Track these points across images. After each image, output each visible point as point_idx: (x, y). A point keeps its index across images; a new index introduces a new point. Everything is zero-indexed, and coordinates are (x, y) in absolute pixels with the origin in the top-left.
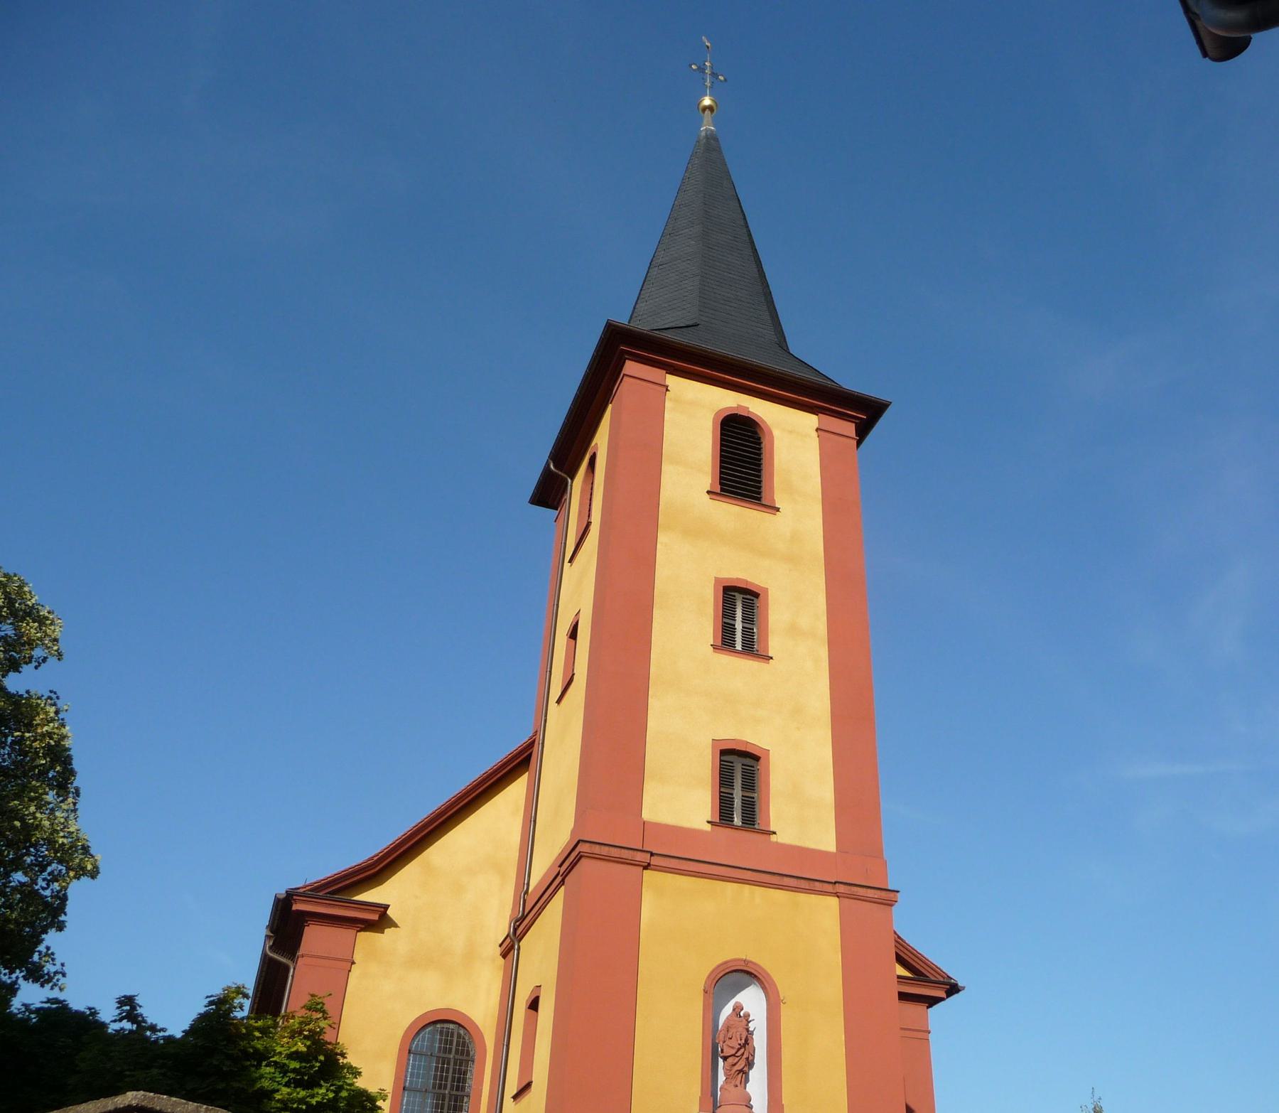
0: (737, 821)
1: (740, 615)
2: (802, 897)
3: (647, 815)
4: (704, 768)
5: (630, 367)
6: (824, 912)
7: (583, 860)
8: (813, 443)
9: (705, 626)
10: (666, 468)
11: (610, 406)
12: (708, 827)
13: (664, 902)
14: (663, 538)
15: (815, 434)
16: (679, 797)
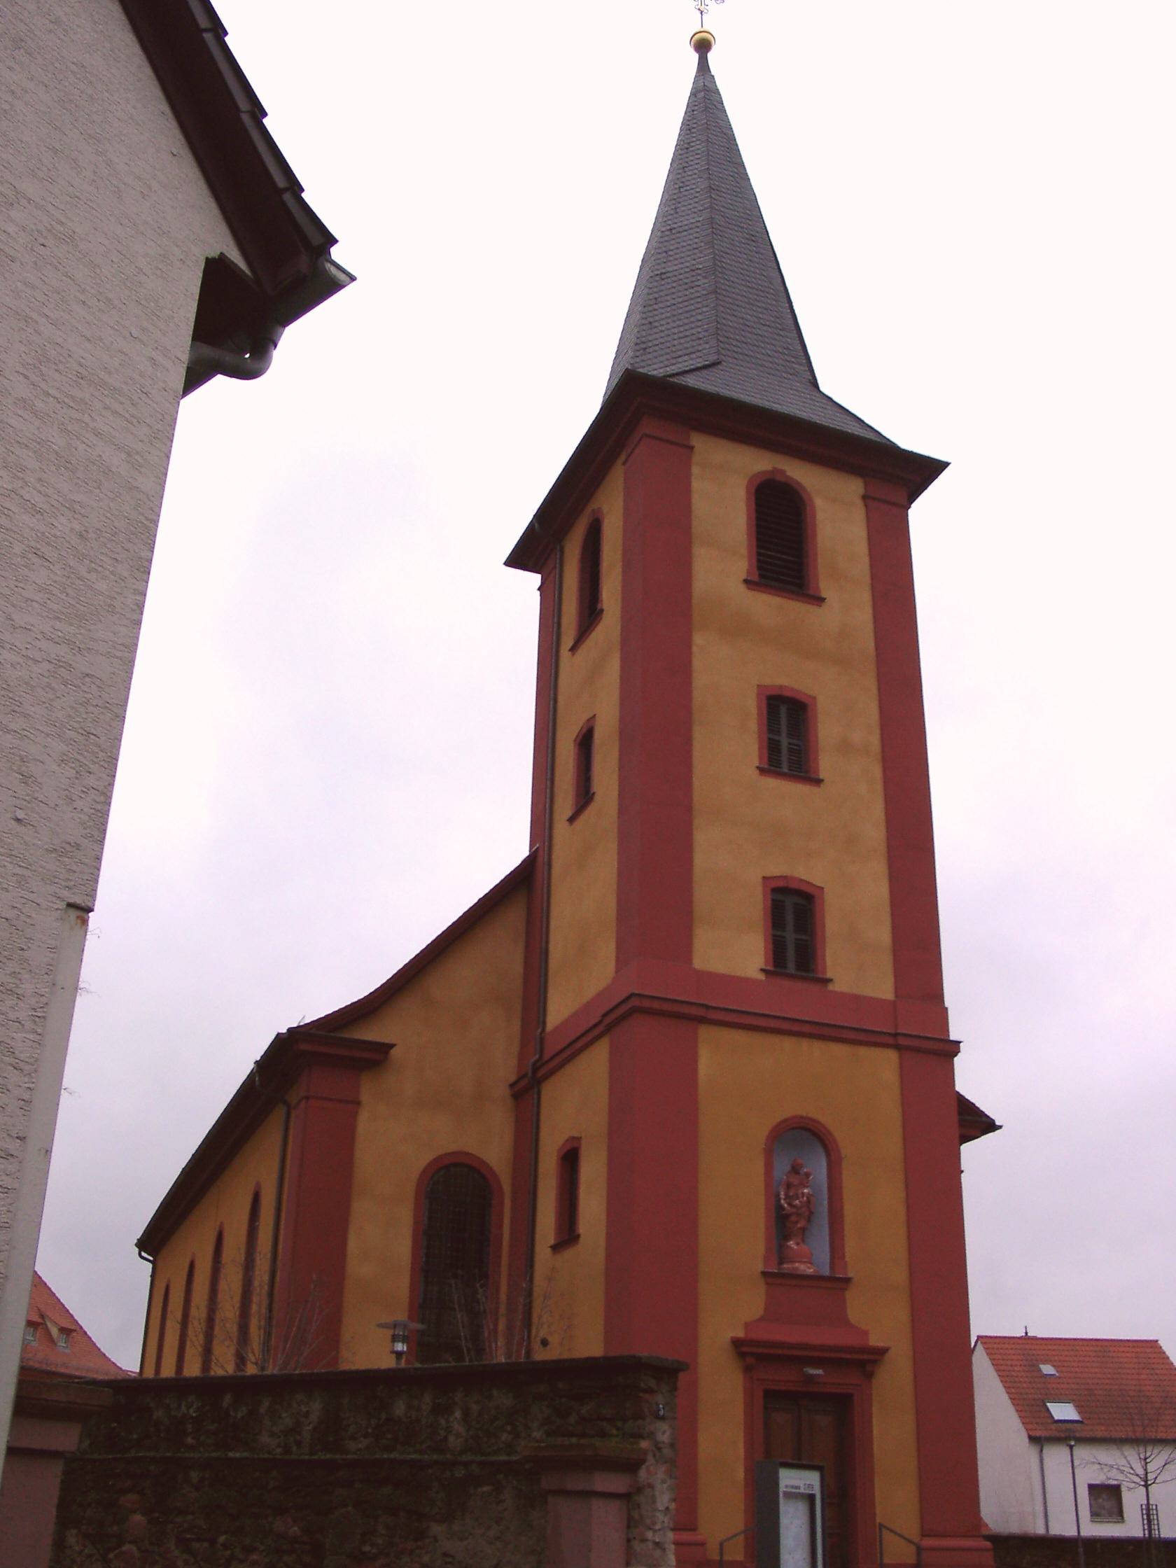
0: (791, 968)
2: (863, 1051)
3: (698, 964)
4: (755, 906)
6: (884, 1066)
8: (859, 513)
9: (828, 729)
12: (762, 977)
13: (718, 1059)
14: (699, 639)
15: (860, 503)
16: (733, 948)
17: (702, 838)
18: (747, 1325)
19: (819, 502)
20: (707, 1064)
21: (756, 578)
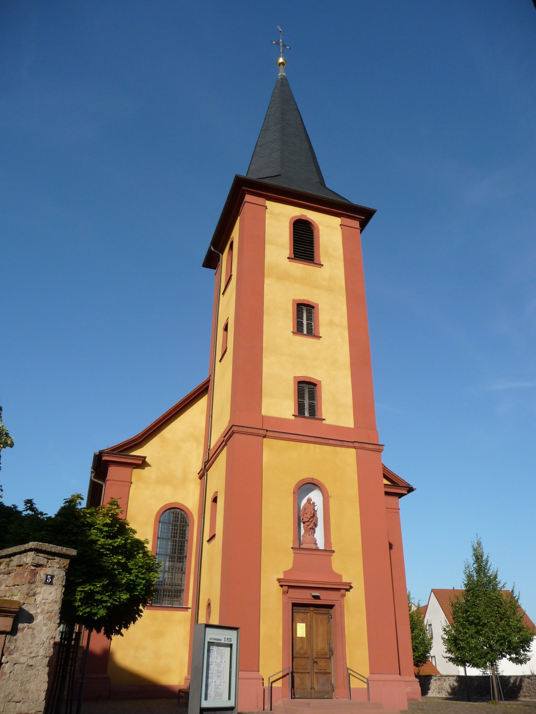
0: (307, 414)
1: (305, 317)
3: (264, 413)
4: (291, 390)
7: (235, 435)
9: (324, 317)
11: (239, 218)
12: (293, 418)
13: (273, 452)
14: (267, 281)
15: (339, 227)
16: (279, 404)
17: (266, 361)
18: (285, 573)
19: (321, 227)
20: (268, 456)
21: (293, 256)
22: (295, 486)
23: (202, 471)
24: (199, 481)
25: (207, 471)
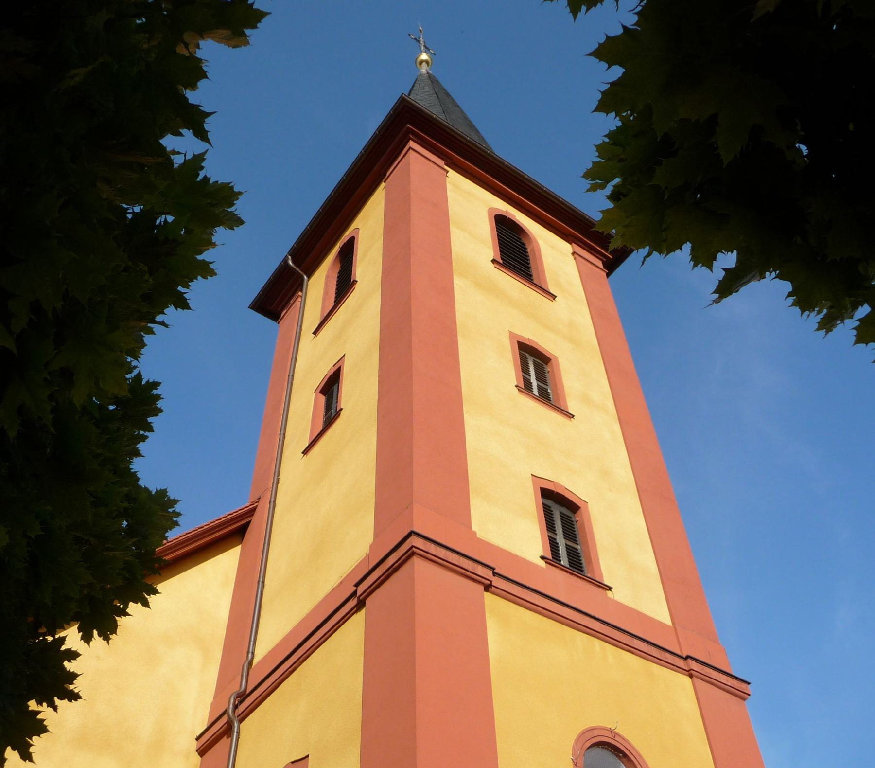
0: (564, 561)
1: (535, 368)
2: (655, 668)
5: (412, 144)
7: (416, 560)
10: (453, 229)
11: (383, 185)
15: (572, 257)
22: (577, 741)
23: (224, 719)
24: (197, 759)
25: (241, 721)
